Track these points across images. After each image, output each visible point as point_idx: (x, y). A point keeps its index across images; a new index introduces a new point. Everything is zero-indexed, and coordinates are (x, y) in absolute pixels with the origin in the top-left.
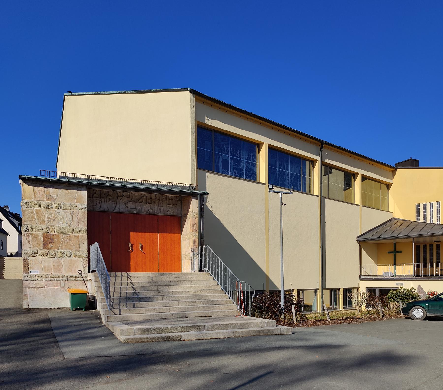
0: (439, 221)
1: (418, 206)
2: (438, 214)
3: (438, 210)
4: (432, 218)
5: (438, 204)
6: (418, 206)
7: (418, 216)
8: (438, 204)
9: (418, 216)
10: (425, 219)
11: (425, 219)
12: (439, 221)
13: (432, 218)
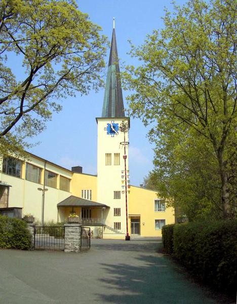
0: (91, 199)
1: (82, 191)
2: (91, 196)
3: (91, 194)
4: (88, 197)
5: (91, 191)
6: (82, 191)
7: (82, 196)
8: (91, 191)
9: (82, 196)
10: (85, 197)
11: (85, 197)
12: (91, 199)
13: (88, 197)
